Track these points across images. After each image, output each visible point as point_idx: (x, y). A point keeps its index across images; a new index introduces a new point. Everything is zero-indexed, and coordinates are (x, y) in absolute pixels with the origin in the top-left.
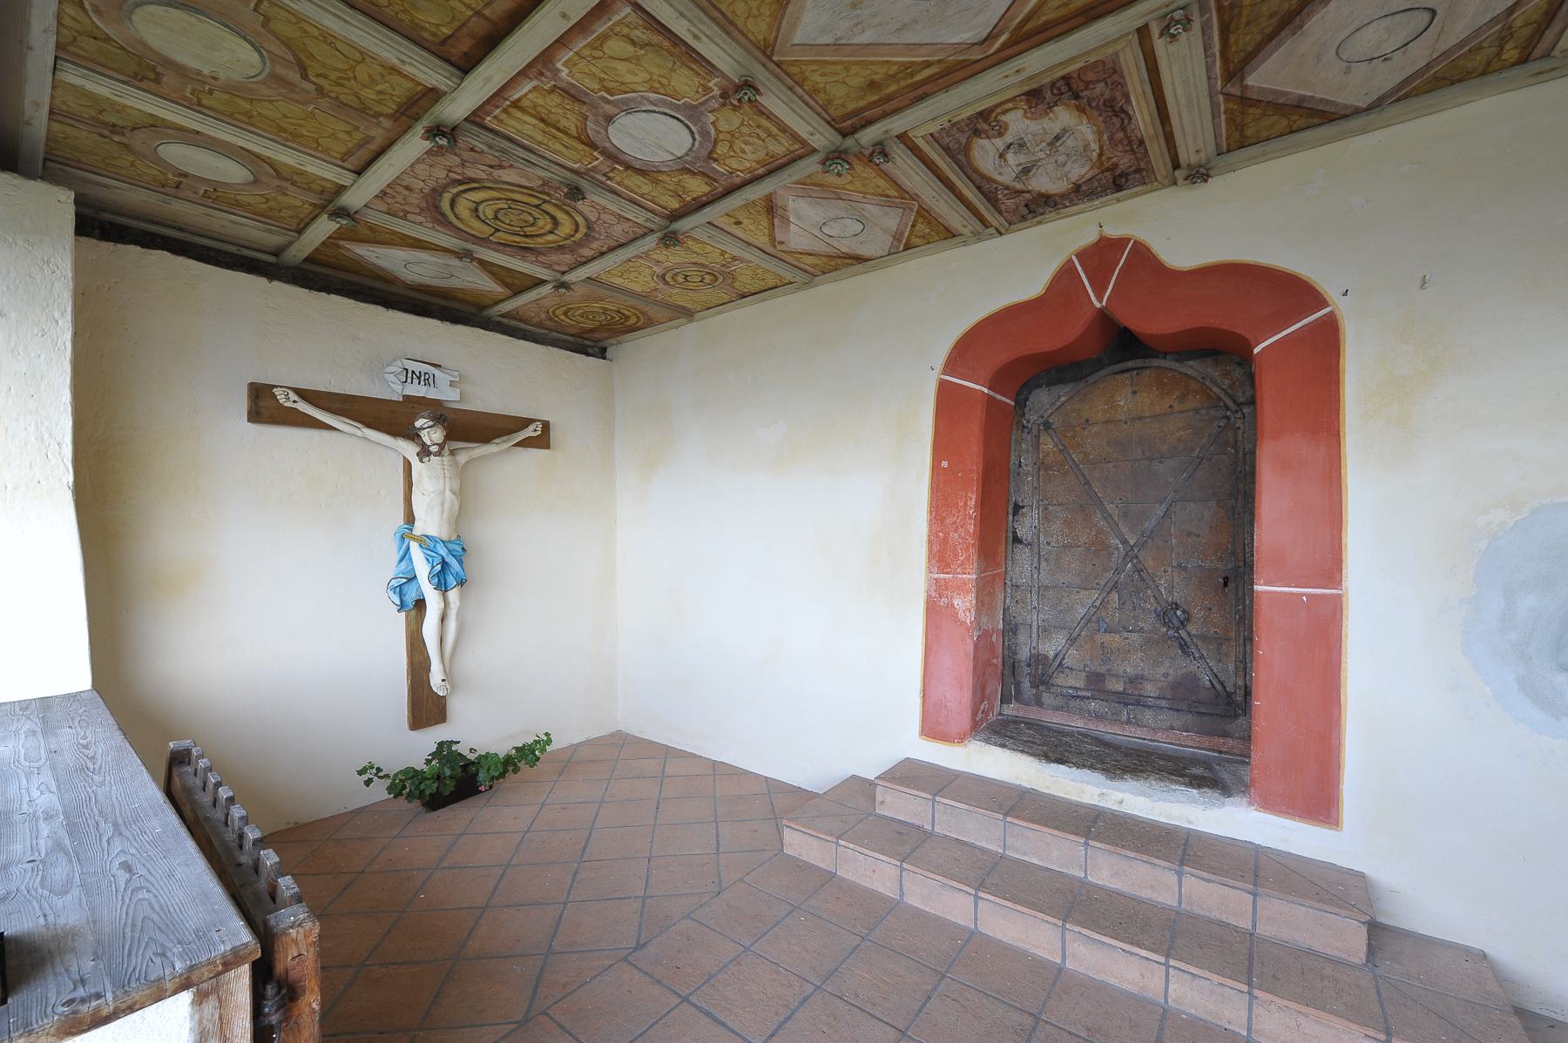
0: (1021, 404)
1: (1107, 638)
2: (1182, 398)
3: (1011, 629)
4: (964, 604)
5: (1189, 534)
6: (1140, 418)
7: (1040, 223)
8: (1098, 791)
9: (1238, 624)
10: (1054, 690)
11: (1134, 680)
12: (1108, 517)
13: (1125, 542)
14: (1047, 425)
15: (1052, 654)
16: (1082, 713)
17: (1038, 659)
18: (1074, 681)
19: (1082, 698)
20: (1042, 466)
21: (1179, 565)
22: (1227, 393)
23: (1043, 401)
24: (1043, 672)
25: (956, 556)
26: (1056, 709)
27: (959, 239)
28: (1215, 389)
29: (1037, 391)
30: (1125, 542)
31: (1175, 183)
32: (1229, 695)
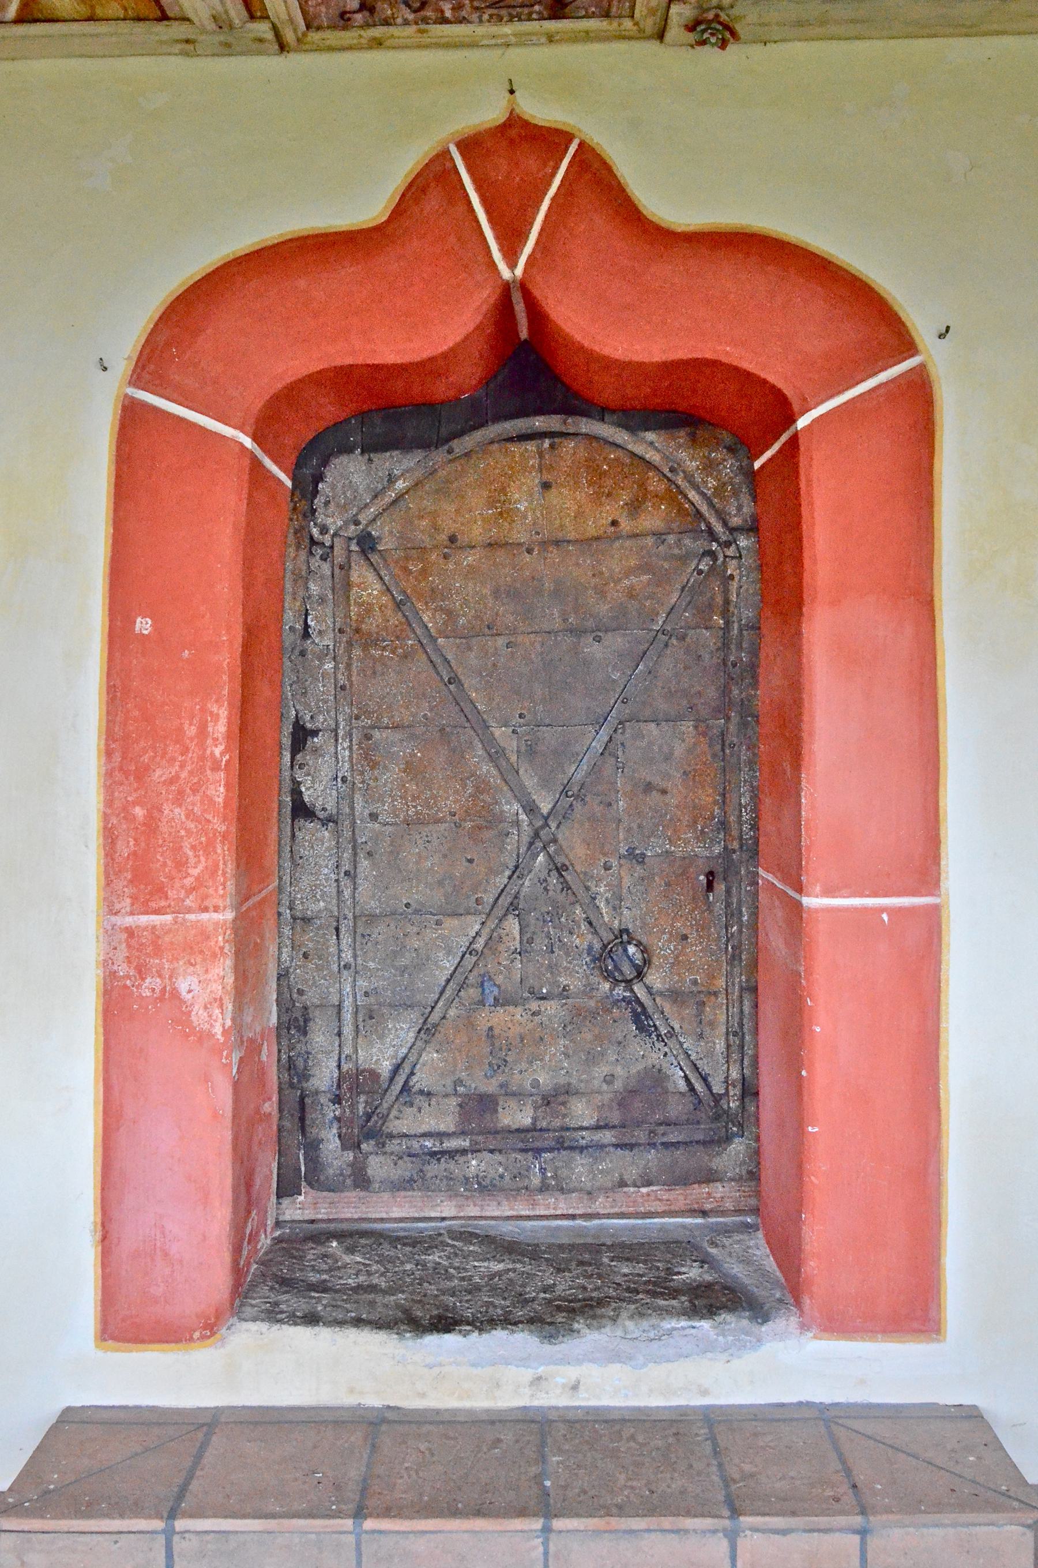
0: (307, 487)
1: (499, 1018)
2: (635, 507)
3: (295, 1022)
4: (205, 989)
5: (649, 787)
6: (557, 543)
7: (378, 43)
8: (527, 1374)
9: (731, 962)
10: (393, 1146)
11: (552, 1099)
12: (495, 755)
13: (531, 809)
14: (367, 543)
15: (385, 1067)
16: (451, 1186)
17: (355, 1082)
18: (438, 1118)
19: (452, 1154)
20: (356, 635)
21: (631, 851)
22: (711, 505)
23: (350, 475)
24: (368, 1105)
25: (181, 864)
26: (405, 1185)
27: (177, 30)
28: (692, 495)
29: (344, 459)
30: (531, 809)
31: (660, 35)
32: (717, 1098)
